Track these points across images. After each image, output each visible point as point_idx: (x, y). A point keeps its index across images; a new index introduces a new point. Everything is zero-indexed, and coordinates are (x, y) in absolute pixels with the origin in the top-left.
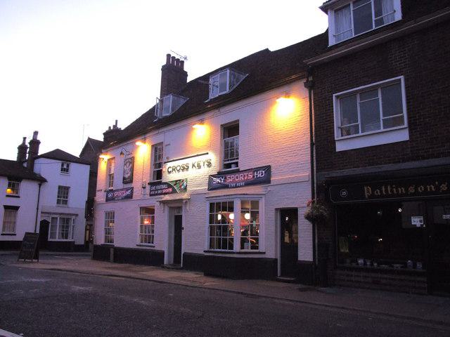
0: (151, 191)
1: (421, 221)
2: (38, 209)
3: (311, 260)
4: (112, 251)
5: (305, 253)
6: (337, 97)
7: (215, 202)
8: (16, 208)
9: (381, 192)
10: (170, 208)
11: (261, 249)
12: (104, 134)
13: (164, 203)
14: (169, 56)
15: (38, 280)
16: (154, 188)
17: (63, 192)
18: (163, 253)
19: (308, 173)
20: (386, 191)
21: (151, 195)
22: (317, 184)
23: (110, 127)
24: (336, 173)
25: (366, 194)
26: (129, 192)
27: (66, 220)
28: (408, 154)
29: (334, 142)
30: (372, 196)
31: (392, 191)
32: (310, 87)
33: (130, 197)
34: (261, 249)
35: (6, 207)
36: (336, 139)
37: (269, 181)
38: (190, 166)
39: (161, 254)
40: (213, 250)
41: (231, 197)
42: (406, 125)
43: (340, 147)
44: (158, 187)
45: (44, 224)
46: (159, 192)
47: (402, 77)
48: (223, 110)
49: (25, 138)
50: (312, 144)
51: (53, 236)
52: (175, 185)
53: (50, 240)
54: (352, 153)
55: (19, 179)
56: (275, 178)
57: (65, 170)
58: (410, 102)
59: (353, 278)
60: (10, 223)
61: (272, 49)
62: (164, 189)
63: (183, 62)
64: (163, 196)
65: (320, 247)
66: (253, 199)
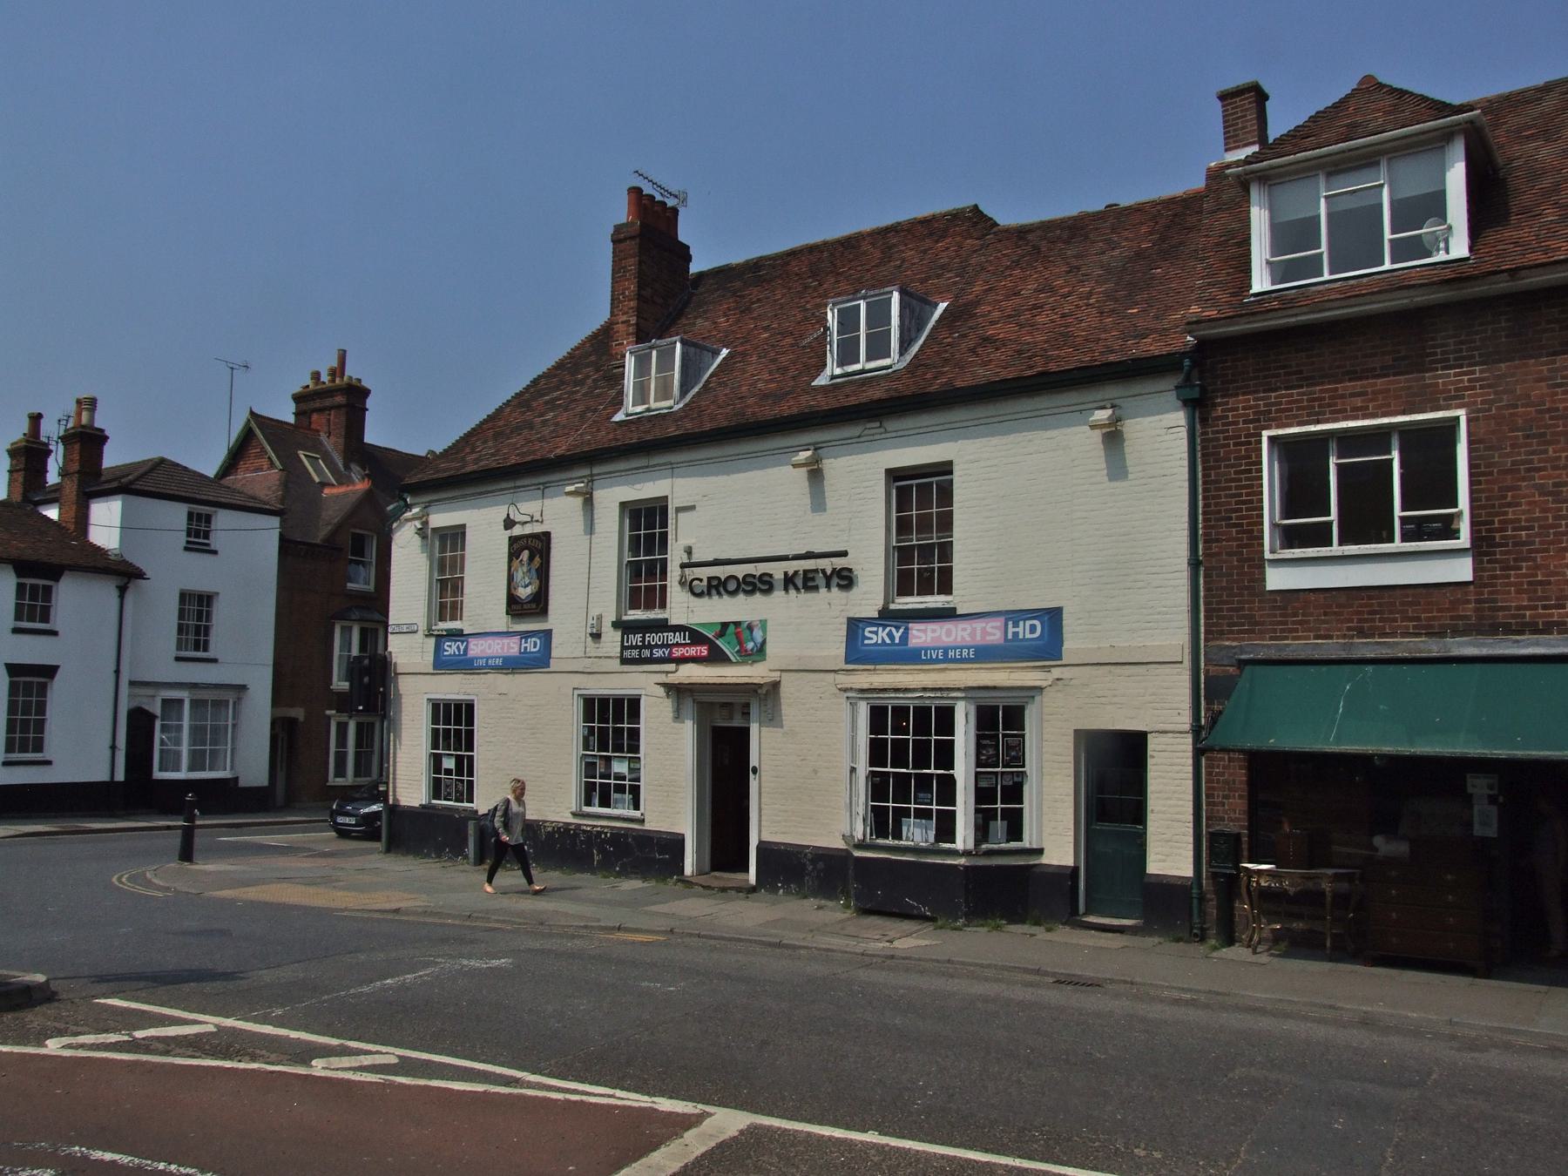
0: (623, 648)
1: (1491, 787)
2: (117, 672)
3: (1188, 871)
5: (1170, 852)
6: (1270, 438)
7: (890, 701)
8: (50, 671)
13: (677, 691)
14: (636, 192)
16: (636, 639)
17: (196, 613)
18: (677, 842)
19: (1182, 637)
21: (624, 661)
22: (1207, 672)
23: (316, 376)
26: (533, 646)
27: (219, 702)
28: (1467, 617)
29: (1259, 564)
32: (1198, 406)
35: (14, 670)
36: (1267, 555)
37: (1057, 655)
39: (675, 844)
40: (880, 841)
42: (1464, 540)
43: (1277, 579)
44: (654, 638)
45: (140, 724)
46: (658, 653)
47: (1462, 413)
48: (893, 425)
49: (36, 419)
50: (1194, 564)
51: (171, 761)
52: (721, 634)
53: (158, 775)
54: (1312, 597)
55: (55, 572)
56: (1074, 643)
57: (198, 538)
58: (1239, 245)
60: (27, 731)
62: (677, 645)
63: (675, 211)
64: (672, 667)
65: (1215, 846)
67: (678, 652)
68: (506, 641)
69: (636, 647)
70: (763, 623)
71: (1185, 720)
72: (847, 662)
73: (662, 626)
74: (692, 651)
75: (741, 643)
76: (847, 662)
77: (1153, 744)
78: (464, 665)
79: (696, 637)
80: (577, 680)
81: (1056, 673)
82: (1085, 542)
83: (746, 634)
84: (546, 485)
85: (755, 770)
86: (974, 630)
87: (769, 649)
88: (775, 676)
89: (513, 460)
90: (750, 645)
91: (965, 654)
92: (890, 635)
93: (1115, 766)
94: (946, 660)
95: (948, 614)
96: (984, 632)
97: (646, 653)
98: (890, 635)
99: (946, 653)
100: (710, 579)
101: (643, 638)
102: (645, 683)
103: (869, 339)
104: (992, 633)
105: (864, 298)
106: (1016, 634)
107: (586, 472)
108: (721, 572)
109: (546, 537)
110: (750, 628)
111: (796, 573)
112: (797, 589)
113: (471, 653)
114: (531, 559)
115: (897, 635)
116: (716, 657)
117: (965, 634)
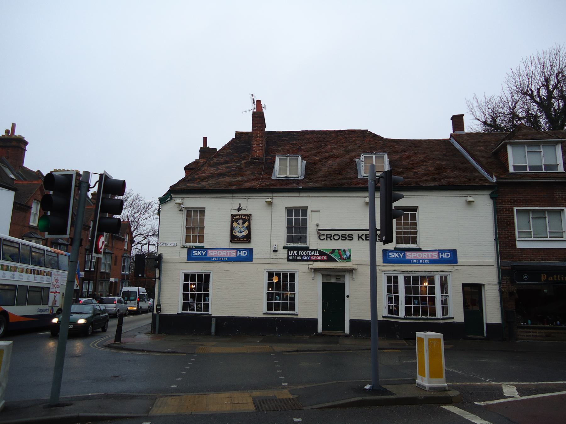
4: (213, 321)
7: (412, 275)
9: (553, 278)
10: (323, 275)
11: (450, 315)
12: (38, 171)
15: (461, 384)
18: (316, 321)
20: (557, 278)
21: (289, 260)
24: (516, 262)
25: (543, 279)
30: (547, 280)
31: (560, 278)
33: (249, 257)
34: (450, 315)
36: (517, 238)
37: (456, 262)
38: (356, 237)
41: (432, 273)
43: (519, 245)
56: (461, 259)
59: (531, 334)
61: (218, 143)
62: (313, 255)
64: (311, 263)
66: (423, 275)
67: (313, 258)
68: (229, 251)
69: (295, 255)
70: (350, 250)
71: (496, 281)
72: (383, 263)
73: (307, 249)
74: (320, 258)
75: (340, 255)
76: (383, 263)
77: (486, 287)
78: (205, 259)
79: (321, 253)
80: (266, 266)
81: (456, 268)
82: (457, 230)
83: (342, 253)
84: (249, 198)
85: (348, 296)
86: (428, 255)
87: (352, 258)
88: (355, 267)
89: (223, 188)
90: (345, 257)
91: (426, 261)
92: (201, 253)
93: (472, 293)
94: (419, 263)
95: (419, 250)
96: (432, 256)
97: (300, 258)
98: (201, 253)
99: (419, 260)
100: (327, 235)
101: (297, 253)
102: (300, 269)
103: (368, 165)
104: (435, 256)
105: (375, 154)
106: (442, 256)
107: (270, 195)
108: (333, 233)
109: (249, 216)
110: (344, 251)
111: (363, 235)
112: (363, 240)
113: (209, 255)
114: (243, 223)
115: (204, 253)
116: (330, 259)
117: (426, 256)
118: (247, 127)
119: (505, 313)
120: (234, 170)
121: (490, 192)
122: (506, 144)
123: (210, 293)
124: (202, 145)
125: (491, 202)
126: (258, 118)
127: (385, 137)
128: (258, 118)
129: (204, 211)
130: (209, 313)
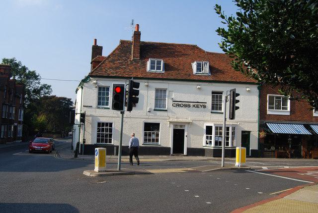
7: (219, 126)
18: (170, 148)
77: (251, 133)
118: (129, 38)
119: (260, 144)
120: (125, 65)
121: (258, 86)
122: (266, 123)
123: (113, 133)
124: (93, 44)
125: (258, 91)
126: (137, 34)
127: (206, 50)
128: (137, 34)
129: (108, 88)
130: (112, 144)
